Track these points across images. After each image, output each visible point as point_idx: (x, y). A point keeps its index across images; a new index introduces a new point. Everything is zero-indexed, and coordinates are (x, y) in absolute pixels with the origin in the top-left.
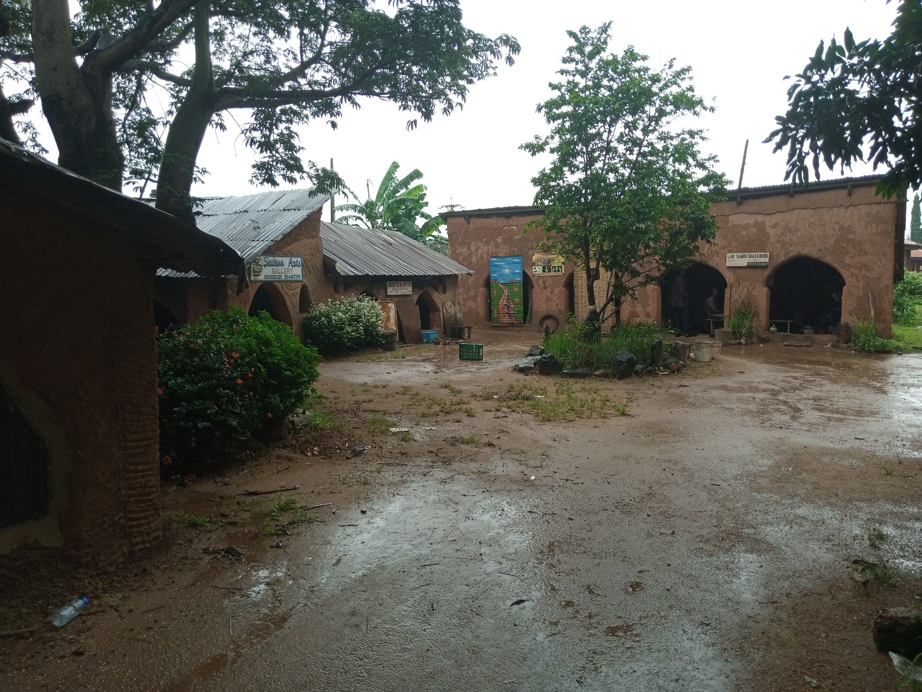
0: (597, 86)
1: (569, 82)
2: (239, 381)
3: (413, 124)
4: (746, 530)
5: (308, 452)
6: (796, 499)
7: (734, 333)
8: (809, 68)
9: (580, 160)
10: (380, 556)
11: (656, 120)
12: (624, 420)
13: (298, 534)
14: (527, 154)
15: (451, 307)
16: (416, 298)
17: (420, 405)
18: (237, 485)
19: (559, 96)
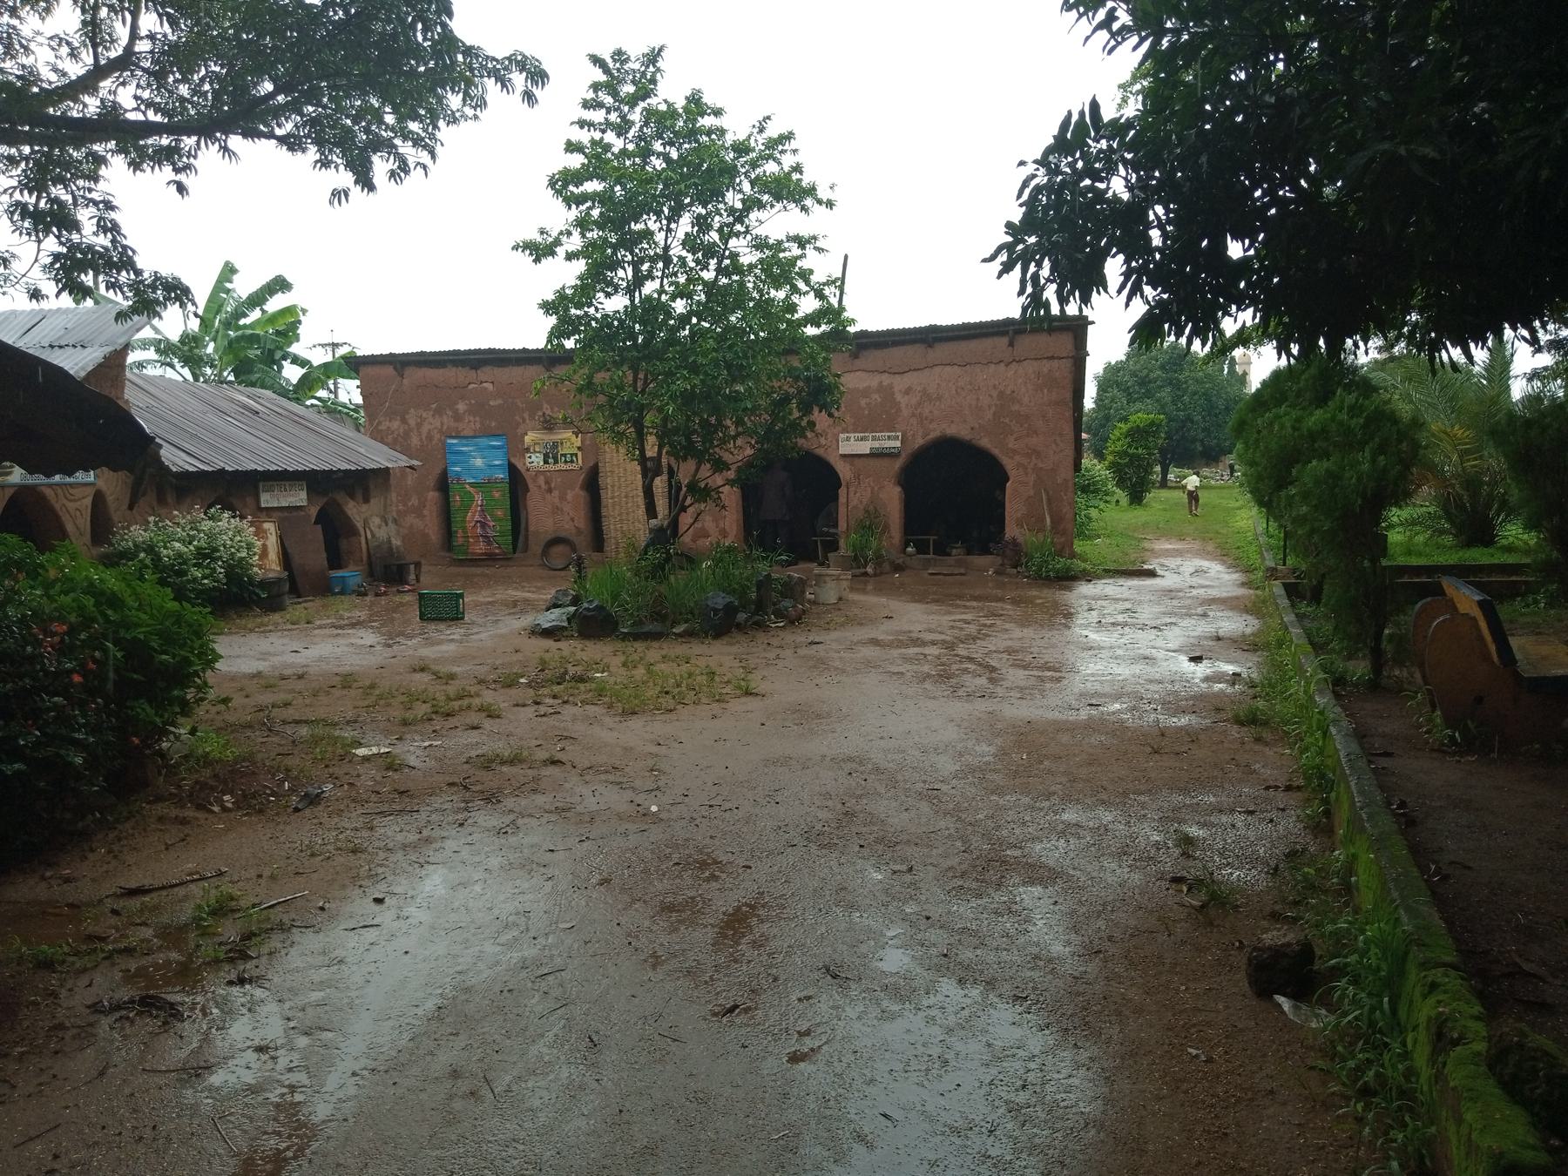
0: (645, 153)
1: (594, 142)
2: (77, 679)
3: (339, 195)
4: (1008, 852)
5: (212, 805)
6: (1055, 800)
7: (856, 558)
8: (1049, 151)
9: (624, 274)
10: (451, 971)
11: (740, 216)
12: (752, 703)
13: (270, 954)
14: (526, 259)
15: (379, 527)
16: (314, 511)
17: (389, 705)
18: (93, 880)
19: (583, 164)
